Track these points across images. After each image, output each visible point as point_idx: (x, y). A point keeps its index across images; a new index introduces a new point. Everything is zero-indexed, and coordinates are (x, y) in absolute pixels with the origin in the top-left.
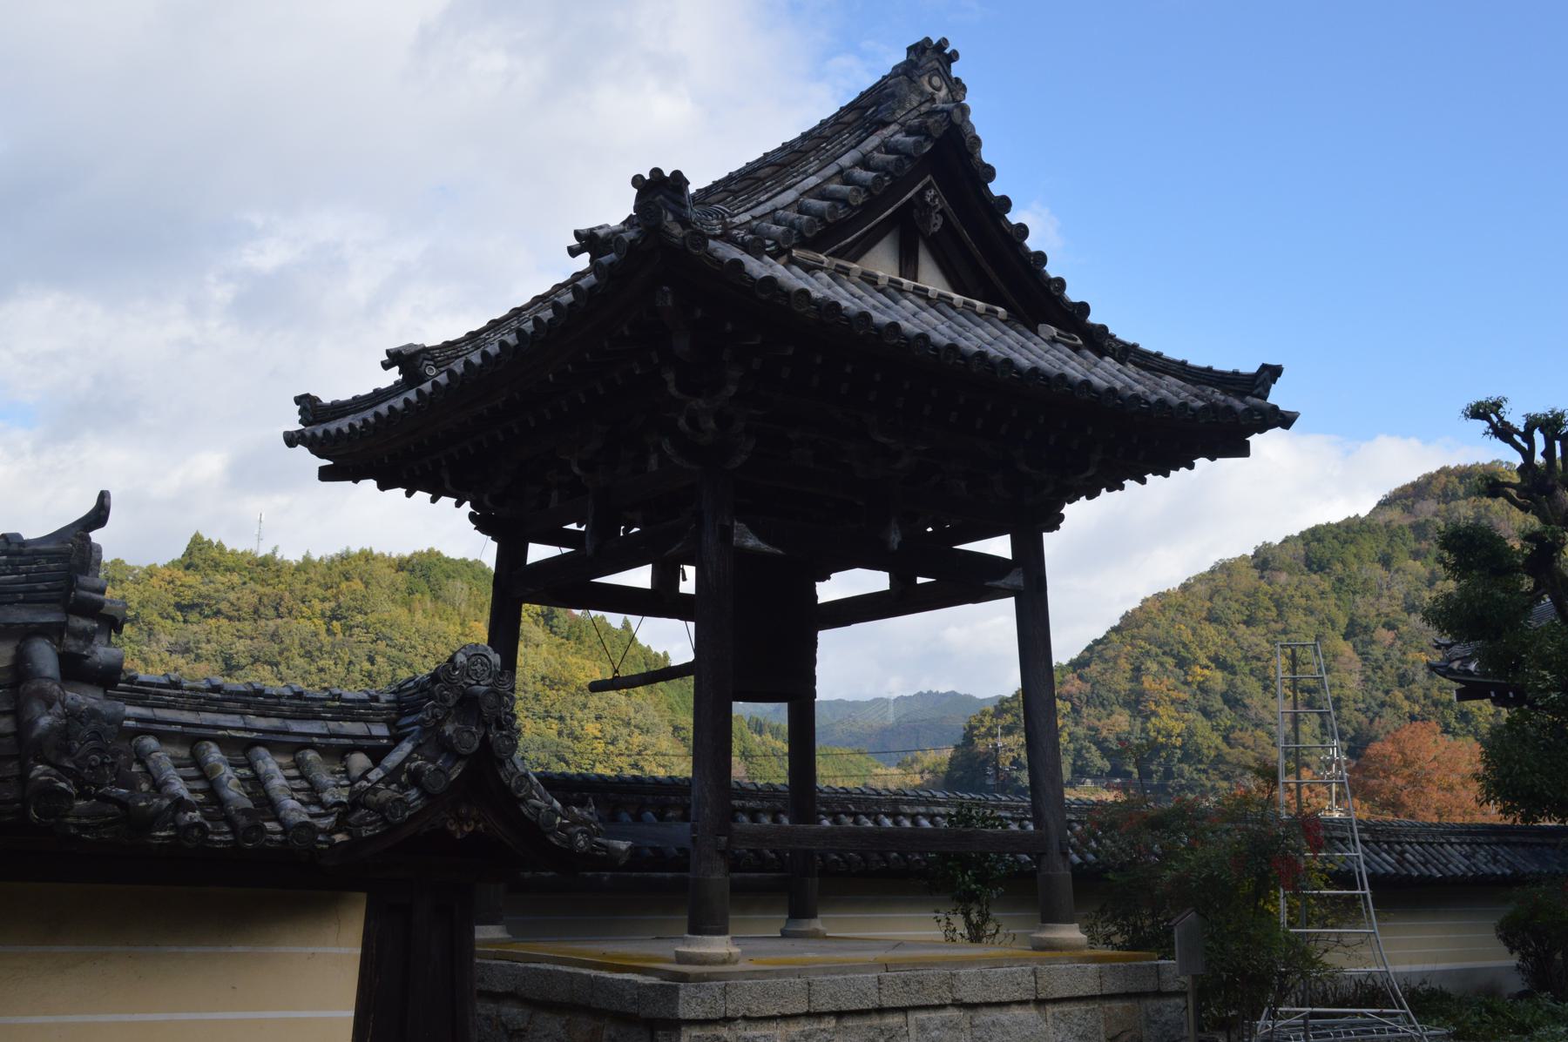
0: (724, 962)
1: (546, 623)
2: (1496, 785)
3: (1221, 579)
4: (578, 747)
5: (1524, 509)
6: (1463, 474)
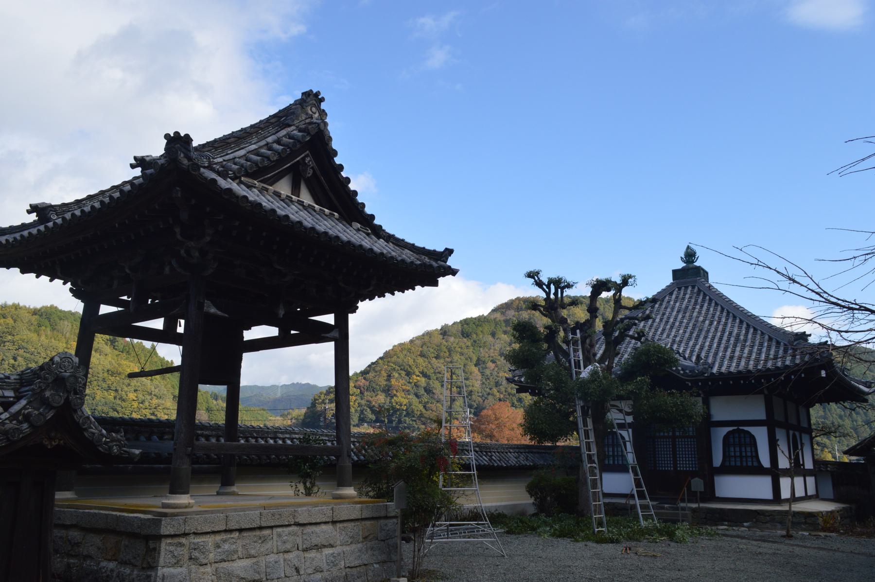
0: (186, 507)
1: (111, 344)
3: (427, 339)
4: (124, 404)
6: (525, 300)
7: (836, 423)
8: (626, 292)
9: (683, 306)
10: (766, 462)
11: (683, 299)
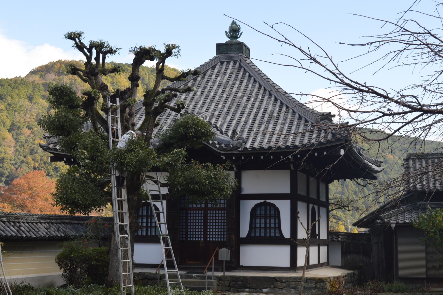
2: (60, 198)
5: (85, 81)
7: (351, 198)
8: (170, 62)
9: (224, 81)
10: (287, 233)
11: (225, 73)
